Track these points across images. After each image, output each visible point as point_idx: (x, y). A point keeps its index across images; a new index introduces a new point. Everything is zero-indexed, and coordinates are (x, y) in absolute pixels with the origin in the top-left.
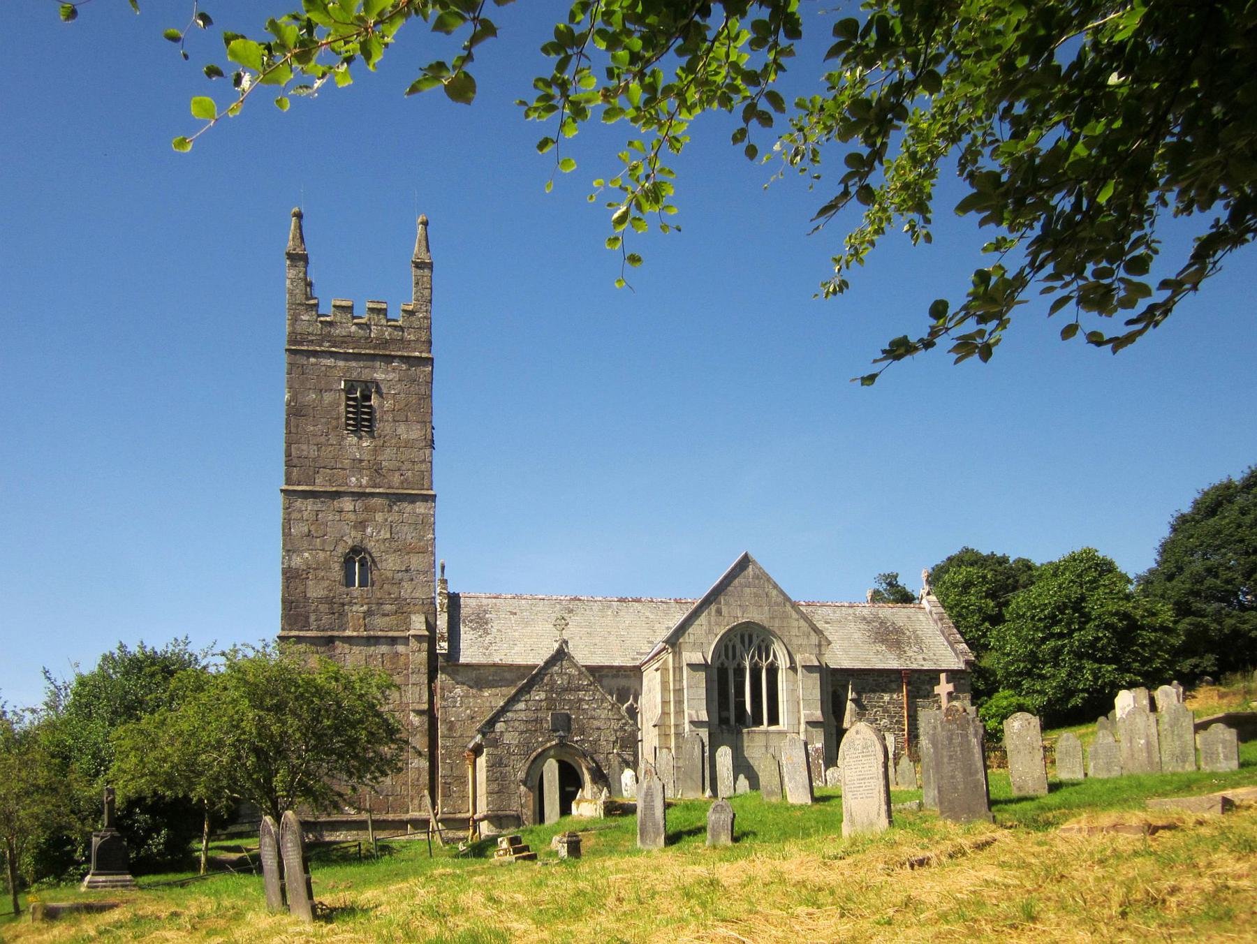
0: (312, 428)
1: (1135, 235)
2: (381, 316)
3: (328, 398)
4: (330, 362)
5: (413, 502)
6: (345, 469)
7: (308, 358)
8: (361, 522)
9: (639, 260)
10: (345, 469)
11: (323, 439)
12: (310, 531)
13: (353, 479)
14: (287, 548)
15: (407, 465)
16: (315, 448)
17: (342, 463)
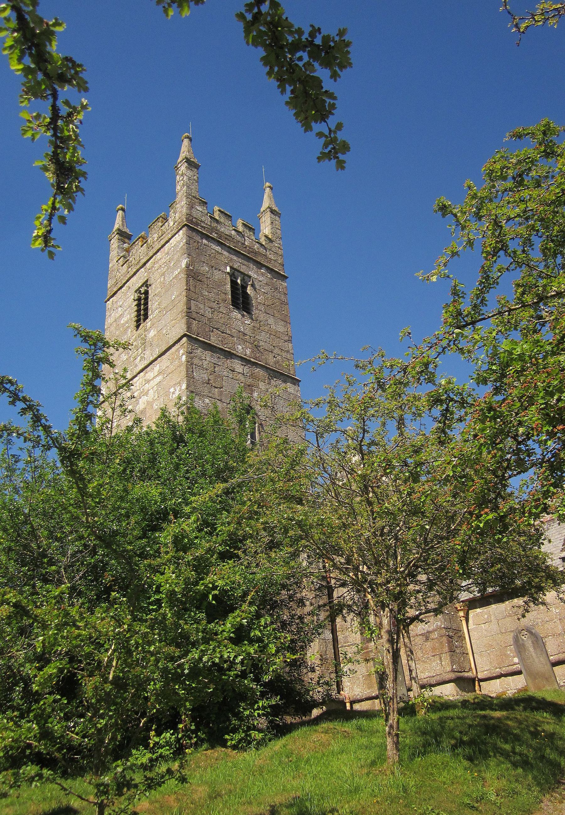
0: (207, 293)
1: (245, 313)
2: (251, 233)
3: (217, 275)
4: (218, 248)
5: (285, 382)
6: (233, 337)
7: (202, 239)
8: (249, 386)
9: (65, 223)
10: (233, 337)
11: (215, 305)
12: (209, 380)
13: (240, 347)
14: (192, 388)
15: (276, 351)
16: (209, 310)
17: (231, 331)
